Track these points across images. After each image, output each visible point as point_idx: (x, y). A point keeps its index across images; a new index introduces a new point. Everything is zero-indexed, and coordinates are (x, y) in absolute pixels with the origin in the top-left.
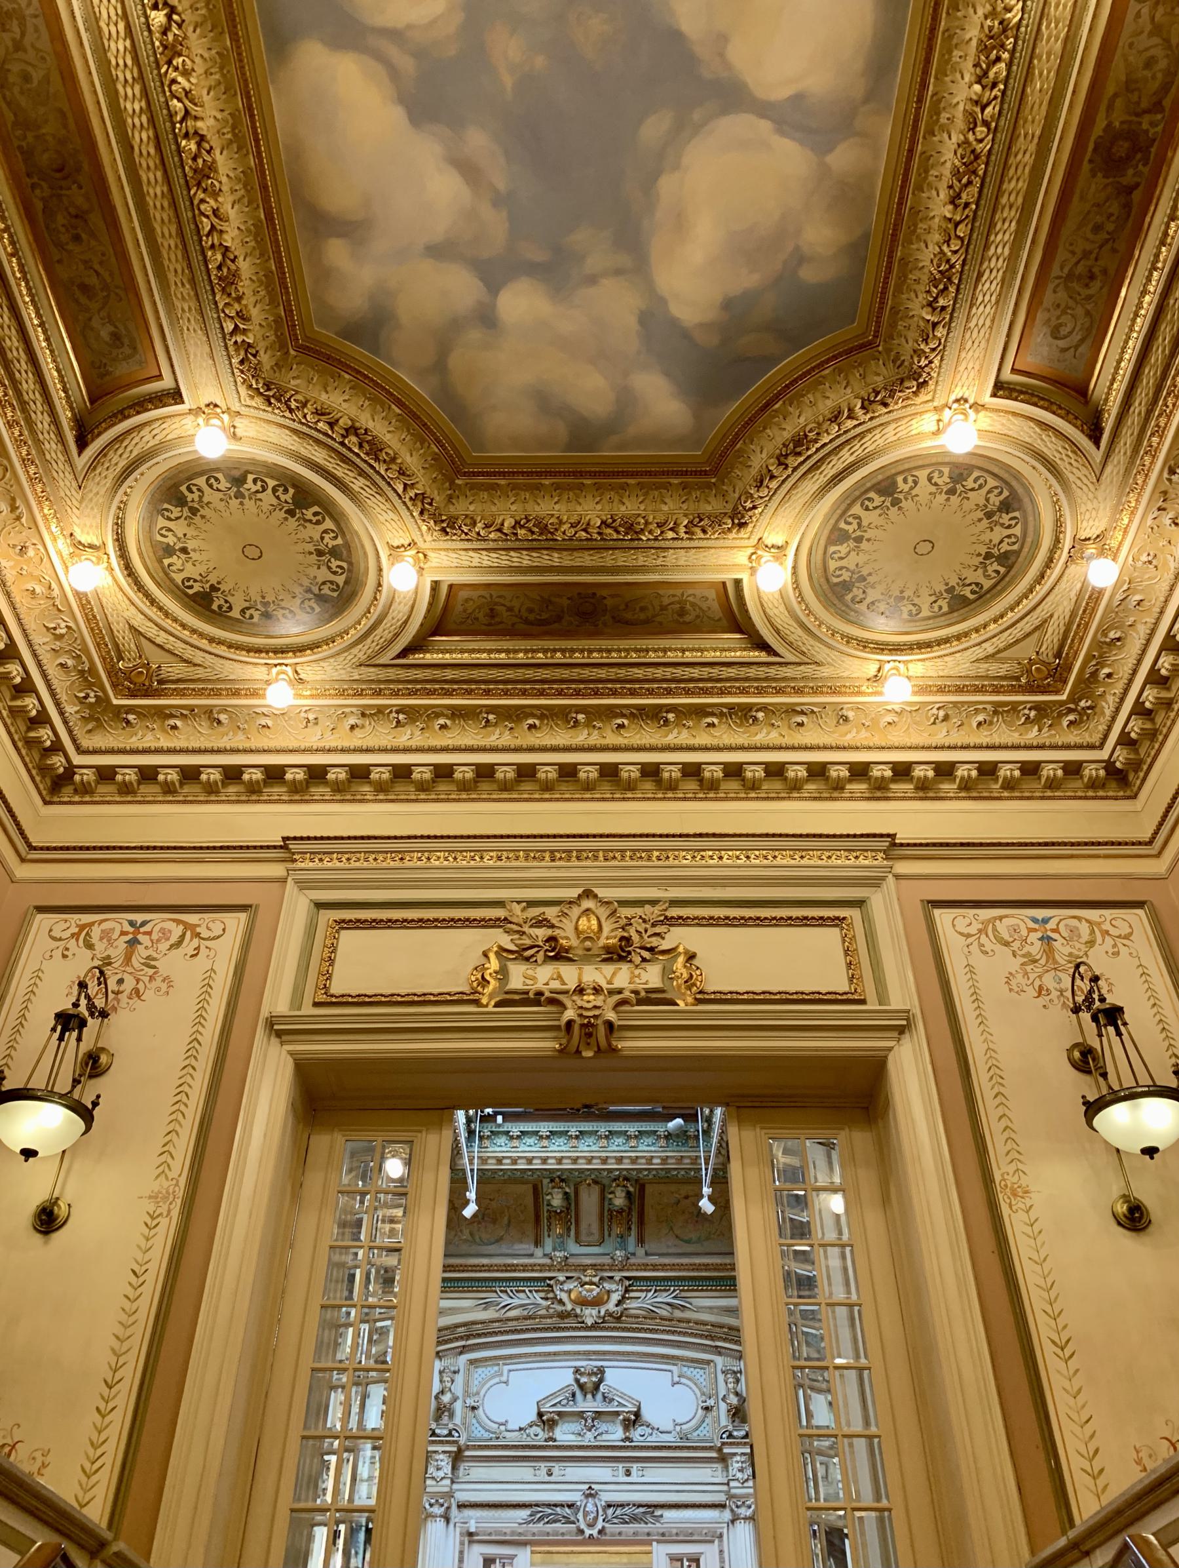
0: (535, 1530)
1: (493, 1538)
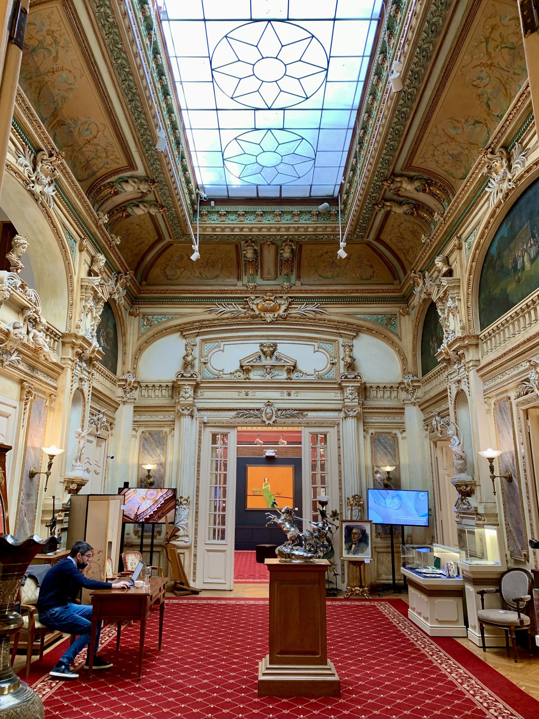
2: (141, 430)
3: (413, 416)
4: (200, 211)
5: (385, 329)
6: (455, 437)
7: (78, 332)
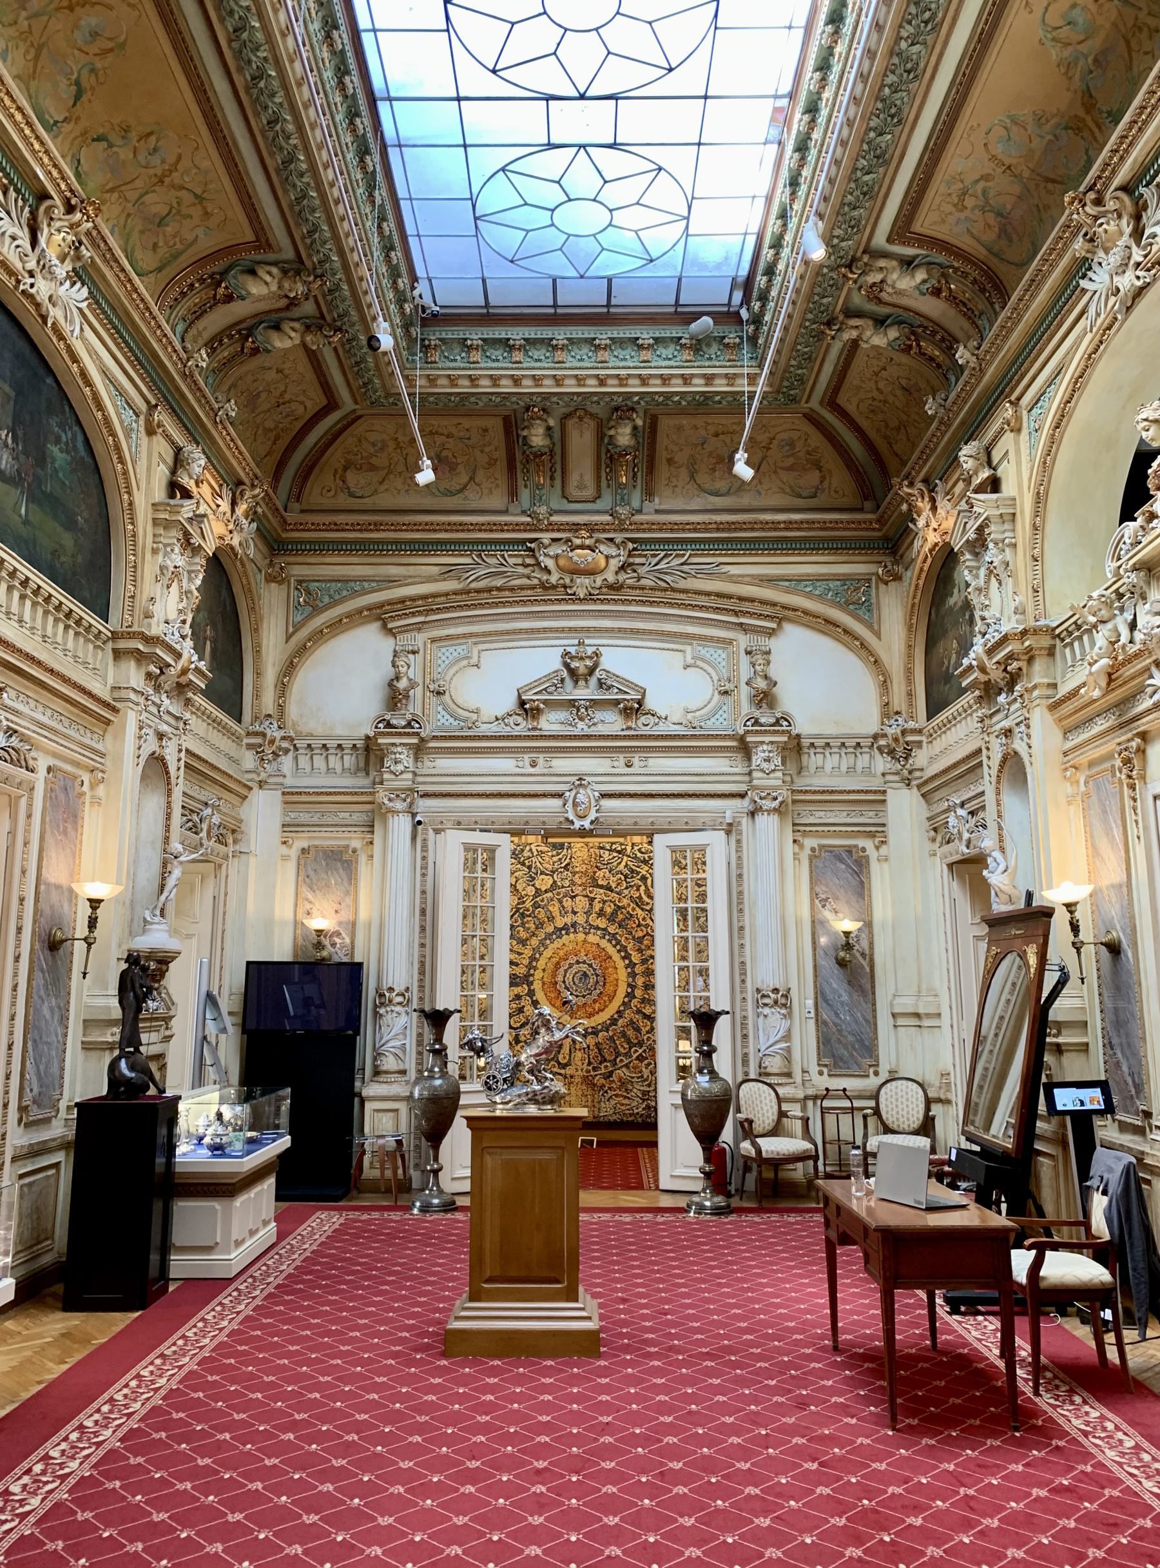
3: (905, 809)
4: (423, 340)
5: (844, 619)
6: (997, 854)
7: (150, 625)
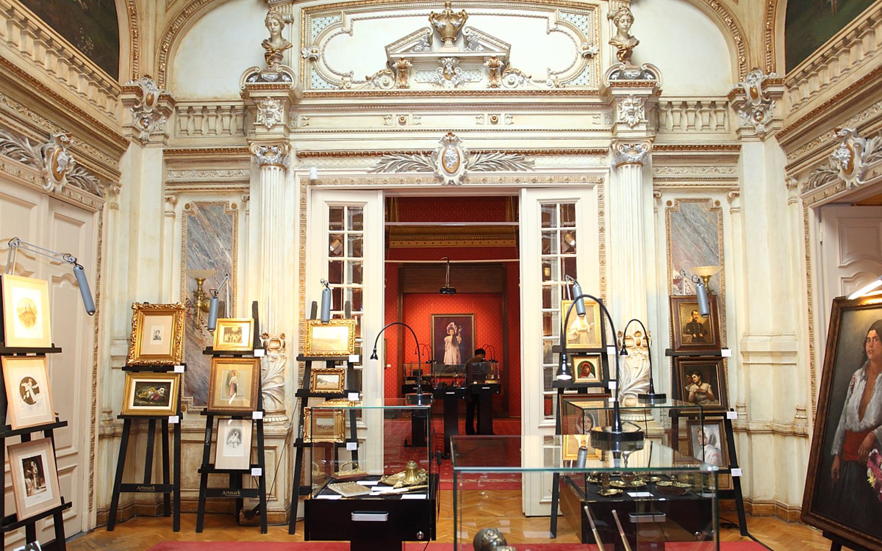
0: (387, 178)
1: (338, 186)
2: (182, 202)
